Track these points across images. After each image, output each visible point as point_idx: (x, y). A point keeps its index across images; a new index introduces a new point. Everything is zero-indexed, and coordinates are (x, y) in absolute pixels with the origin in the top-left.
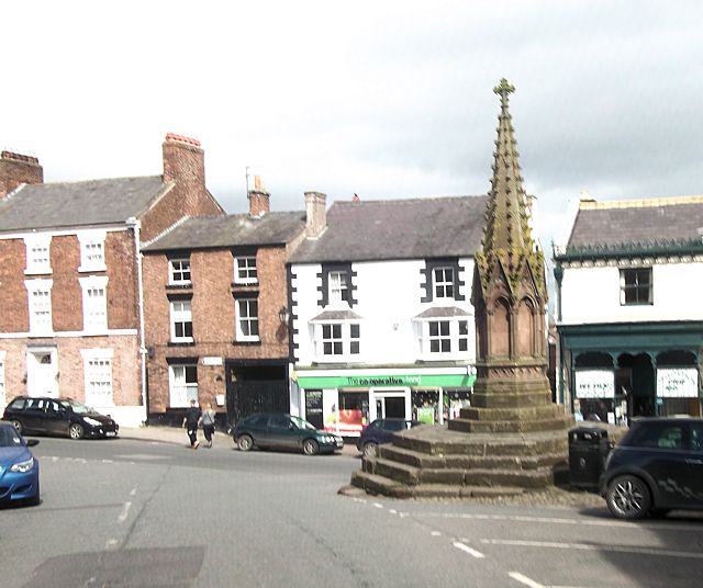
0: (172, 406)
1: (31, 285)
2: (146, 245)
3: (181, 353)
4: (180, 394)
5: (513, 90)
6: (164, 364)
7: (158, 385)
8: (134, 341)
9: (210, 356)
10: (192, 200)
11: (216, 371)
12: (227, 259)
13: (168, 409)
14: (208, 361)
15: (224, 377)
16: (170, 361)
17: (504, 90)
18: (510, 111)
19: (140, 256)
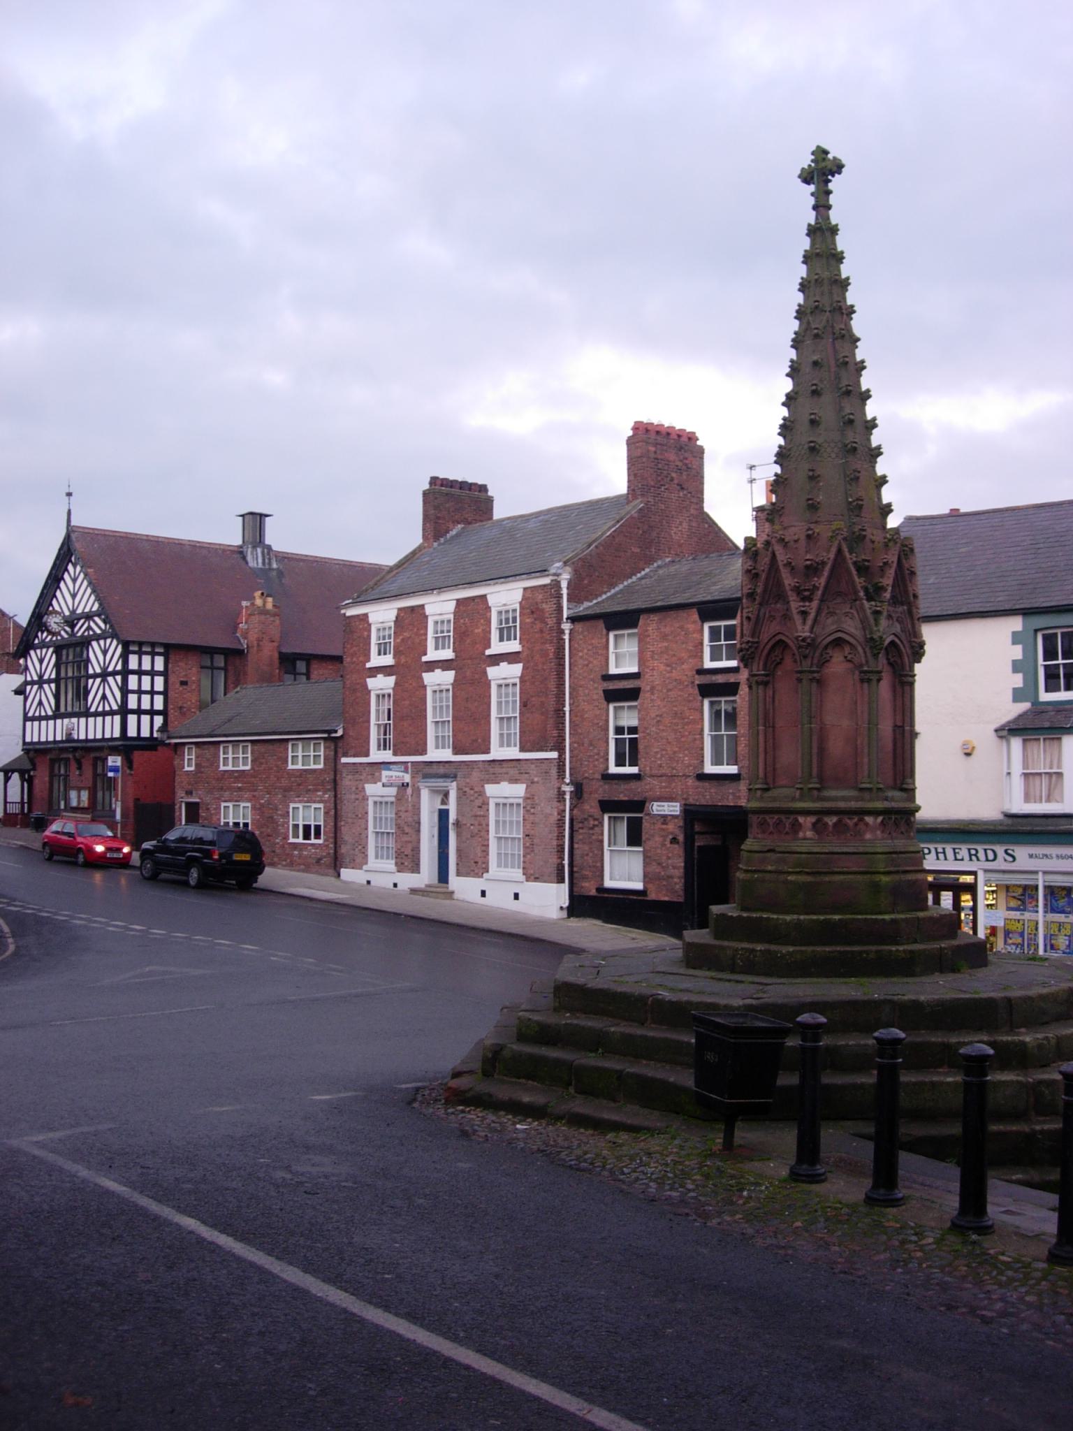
0: (608, 883)
1: (494, 673)
2: (584, 607)
3: (622, 793)
4: (623, 871)
5: (838, 167)
6: (596, 811)
7: (586, 848)
8: (554, 772)
9: (659, 799)
10: (679, 530)
11: (671, 827)
12: (691, 627)
13: (601, 890)
14: (658, 808)
15: (681, 838)
16: (607, 806)
17: (822, 171)
18: (835, 217)
19: (566, 627)
